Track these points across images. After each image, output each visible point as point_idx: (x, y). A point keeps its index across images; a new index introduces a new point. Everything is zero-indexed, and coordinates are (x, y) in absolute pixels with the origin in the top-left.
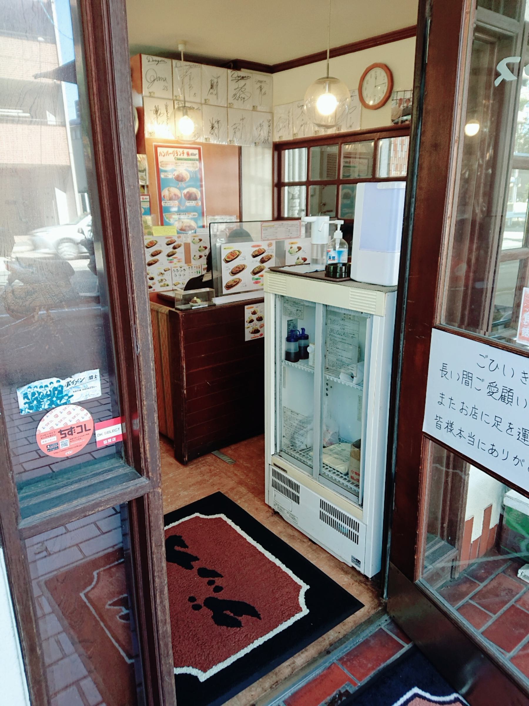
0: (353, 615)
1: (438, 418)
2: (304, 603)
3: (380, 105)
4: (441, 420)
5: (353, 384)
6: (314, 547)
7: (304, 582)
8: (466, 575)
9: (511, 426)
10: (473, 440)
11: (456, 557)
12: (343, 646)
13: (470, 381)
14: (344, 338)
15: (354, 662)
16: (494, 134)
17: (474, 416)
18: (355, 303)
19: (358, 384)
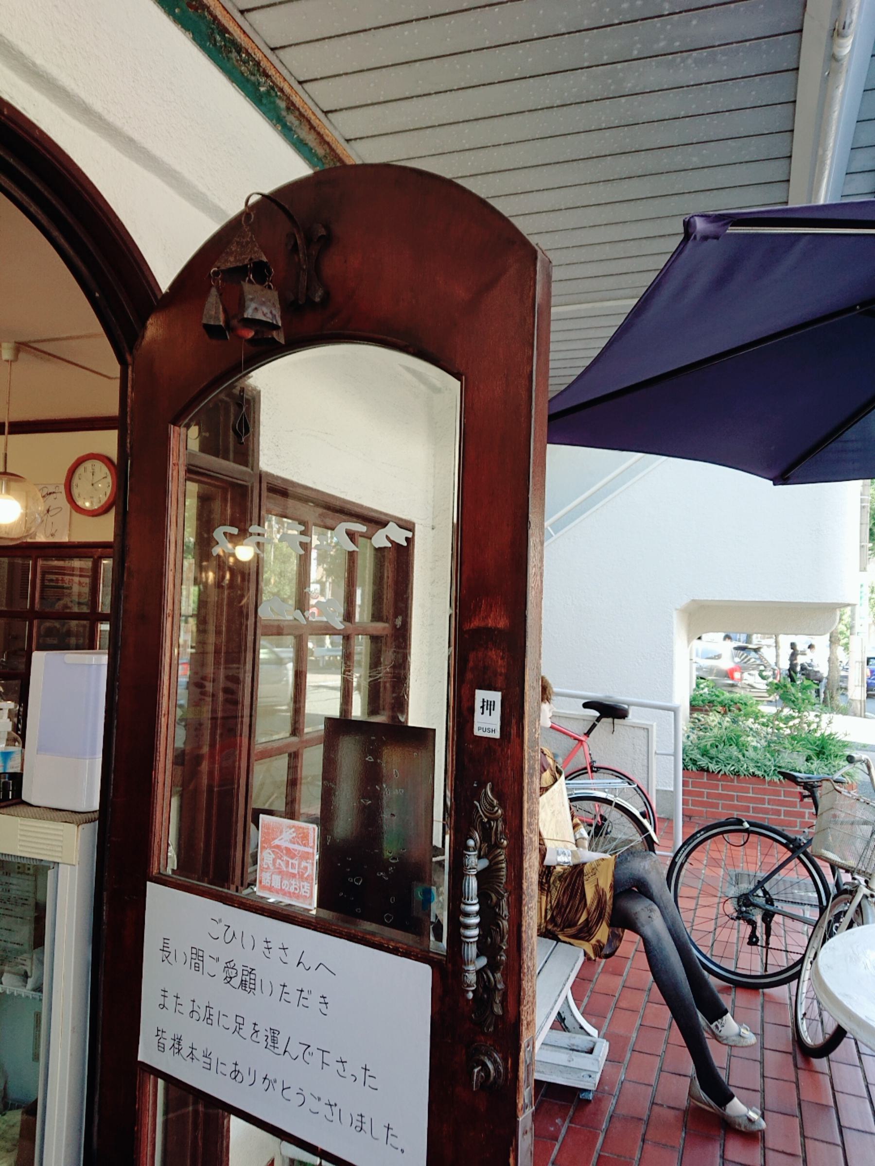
3: (100, 511)
4: (164, 1035)
5: (27, 991)
9: (257, 1028)
13: (201, 963)
14: (10, 907)
17: (209, 1021)
18: (39, 835)
19: (35, 990)
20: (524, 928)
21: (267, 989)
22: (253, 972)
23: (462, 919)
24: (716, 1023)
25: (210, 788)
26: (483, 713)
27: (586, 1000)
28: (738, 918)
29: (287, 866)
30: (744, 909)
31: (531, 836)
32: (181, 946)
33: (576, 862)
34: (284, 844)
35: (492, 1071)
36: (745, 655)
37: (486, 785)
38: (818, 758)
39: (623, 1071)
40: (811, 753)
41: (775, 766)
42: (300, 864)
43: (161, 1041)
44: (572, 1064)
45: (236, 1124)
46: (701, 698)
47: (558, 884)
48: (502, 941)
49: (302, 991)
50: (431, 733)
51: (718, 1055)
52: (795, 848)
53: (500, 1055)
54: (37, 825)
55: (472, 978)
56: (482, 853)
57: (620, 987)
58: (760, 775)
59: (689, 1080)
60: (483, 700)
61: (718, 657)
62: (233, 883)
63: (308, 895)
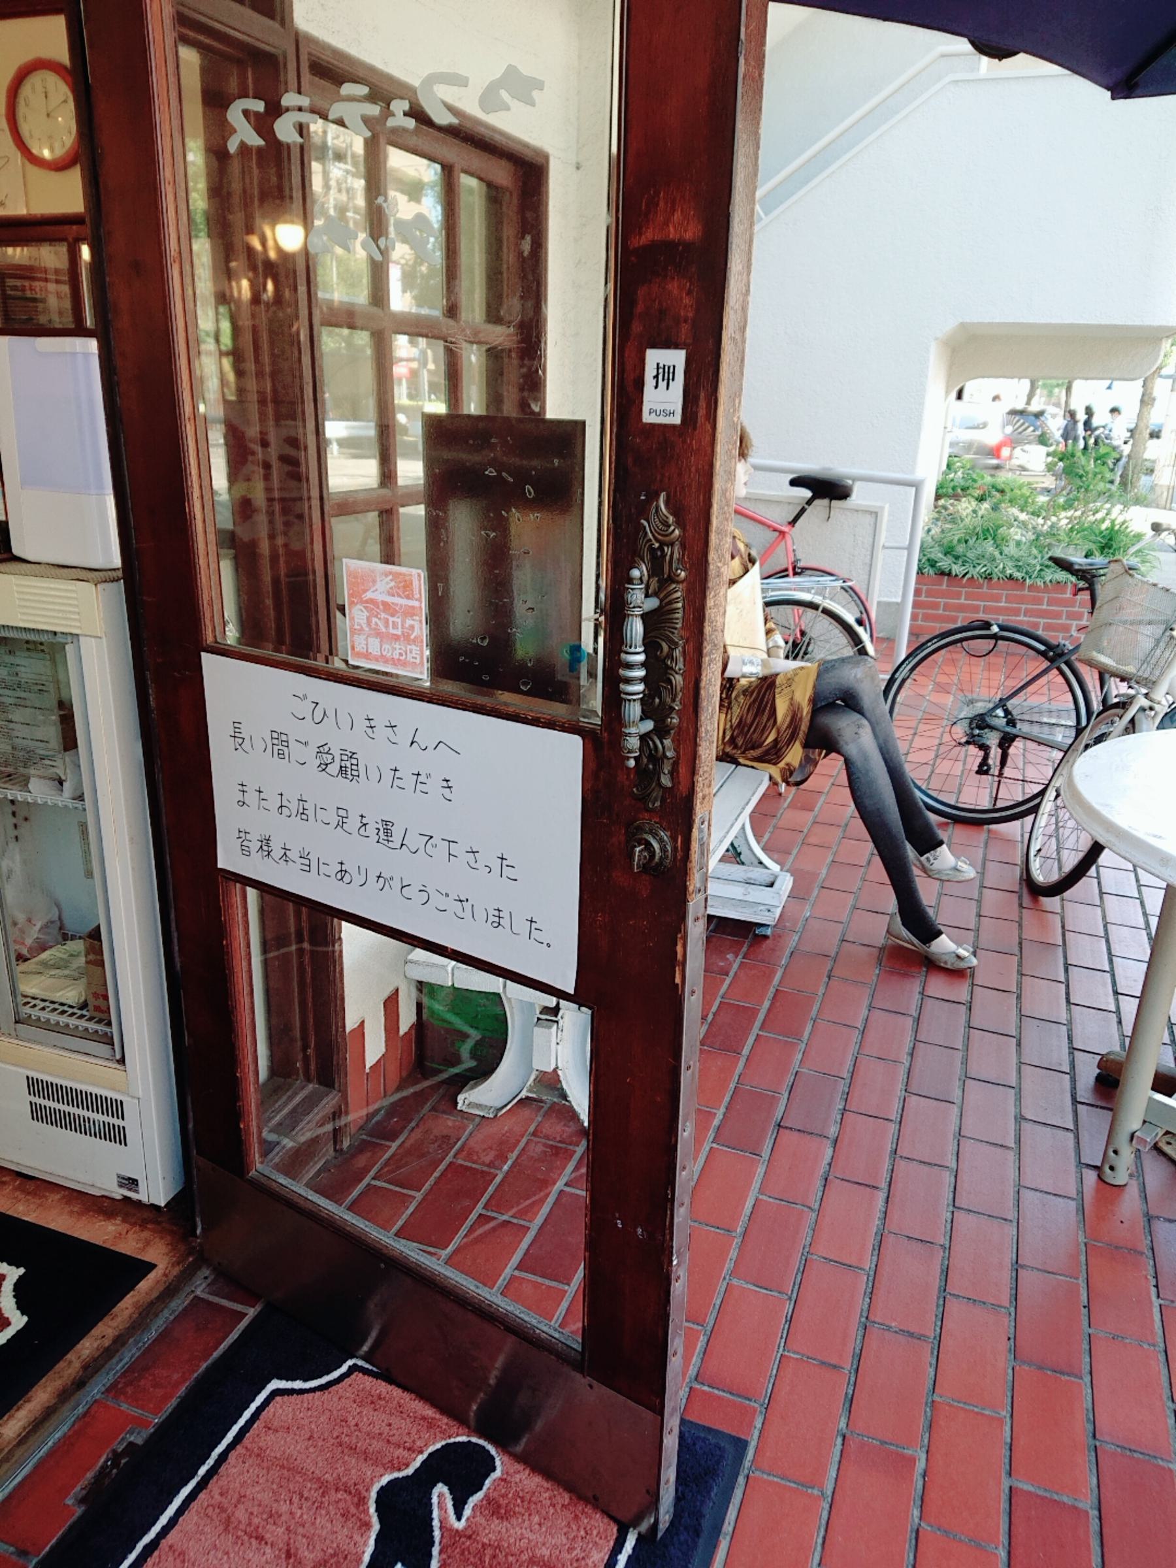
0: (132, 1293)
1: (243, 834)
2: (15, 1306)
4: (248, 837)
5: (65, 798)
6: (31, 1186)
7: (10, 1264)
8: (364, 1137)
9: (365, 821)
10: (307, 862)
11: (340, 1106)
12: (114, 1360)
13: (285, 749)
14: (23, 695)
15: (142, 1383)
16: (110, 316)
17: (304, 817)
20: (703, 684)
21: (374, 776)
22: (354, 756)
23: (622, 672)
24: (927, 855)
25: (276, 581)
26: (656, 387)
27: (767, 836)
28: (968, 743)
29: (387, 626)
30: (977, 732)
31: (719, 564)
32: (257, 730)
33: (767, 672)
34: (380, 597)
35: (657, 850)
36: (1022, 421)
37: (659, 495)
38: (1102, 553)
39: (808, 907)
40: (1093, 547)
41: (1041, 565)
42: (403, 622)
43: (245, 843)
44: (749, 898)
45: (348, 930)
46: (952, 484)
47: (741, 699)
48: (673, 700)
49: (418, 775)
50: (580, 427)
51: (927, 892)
52: (1054, 655)
53: (668, 833)
54: (39, 585)
55: (634, 743)
56: (650, 592)
57: (809, 823)
58: (1020, 578)
59: (888, 917)
60: (658, 364)
61: (984, 426)
62: (319, 651)
63: (418, 661)
